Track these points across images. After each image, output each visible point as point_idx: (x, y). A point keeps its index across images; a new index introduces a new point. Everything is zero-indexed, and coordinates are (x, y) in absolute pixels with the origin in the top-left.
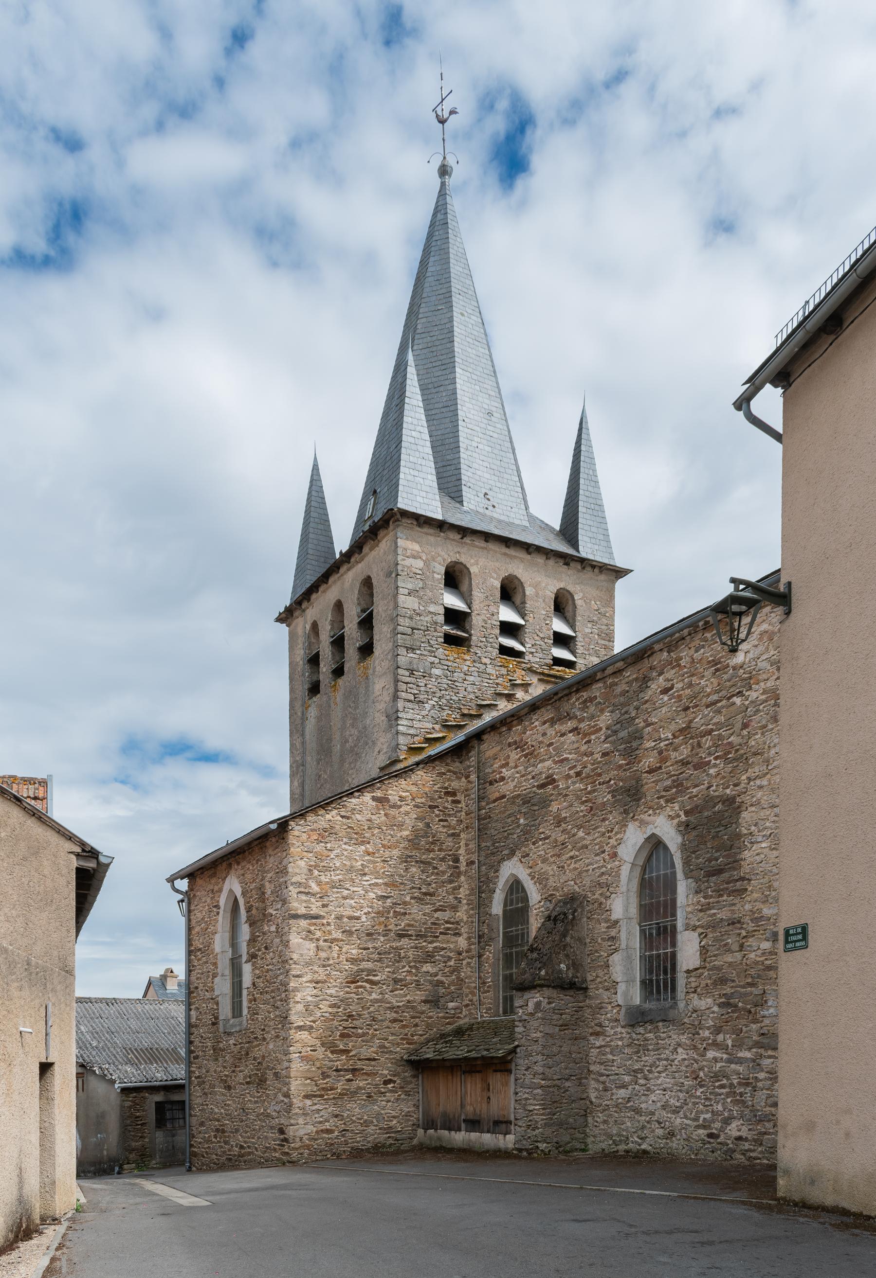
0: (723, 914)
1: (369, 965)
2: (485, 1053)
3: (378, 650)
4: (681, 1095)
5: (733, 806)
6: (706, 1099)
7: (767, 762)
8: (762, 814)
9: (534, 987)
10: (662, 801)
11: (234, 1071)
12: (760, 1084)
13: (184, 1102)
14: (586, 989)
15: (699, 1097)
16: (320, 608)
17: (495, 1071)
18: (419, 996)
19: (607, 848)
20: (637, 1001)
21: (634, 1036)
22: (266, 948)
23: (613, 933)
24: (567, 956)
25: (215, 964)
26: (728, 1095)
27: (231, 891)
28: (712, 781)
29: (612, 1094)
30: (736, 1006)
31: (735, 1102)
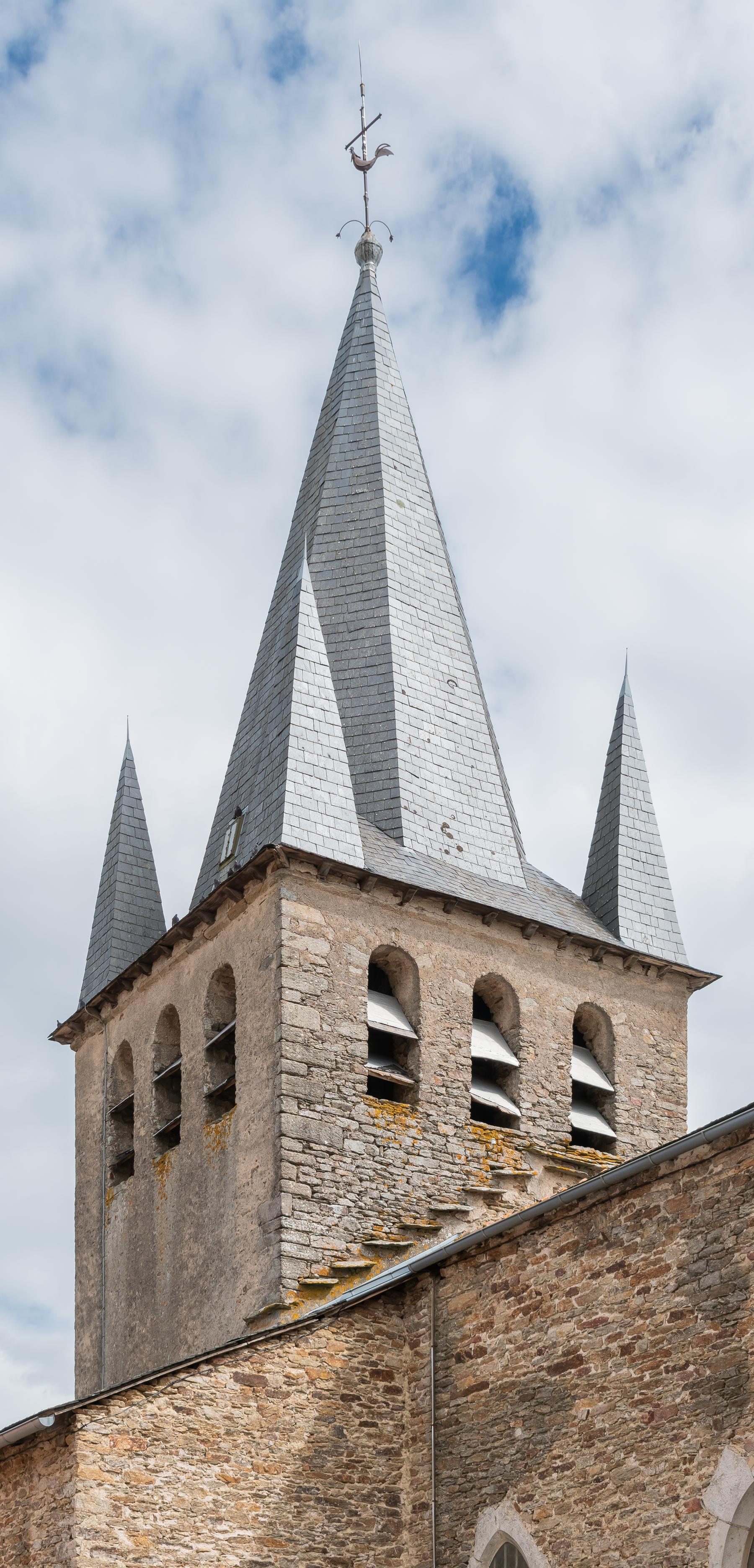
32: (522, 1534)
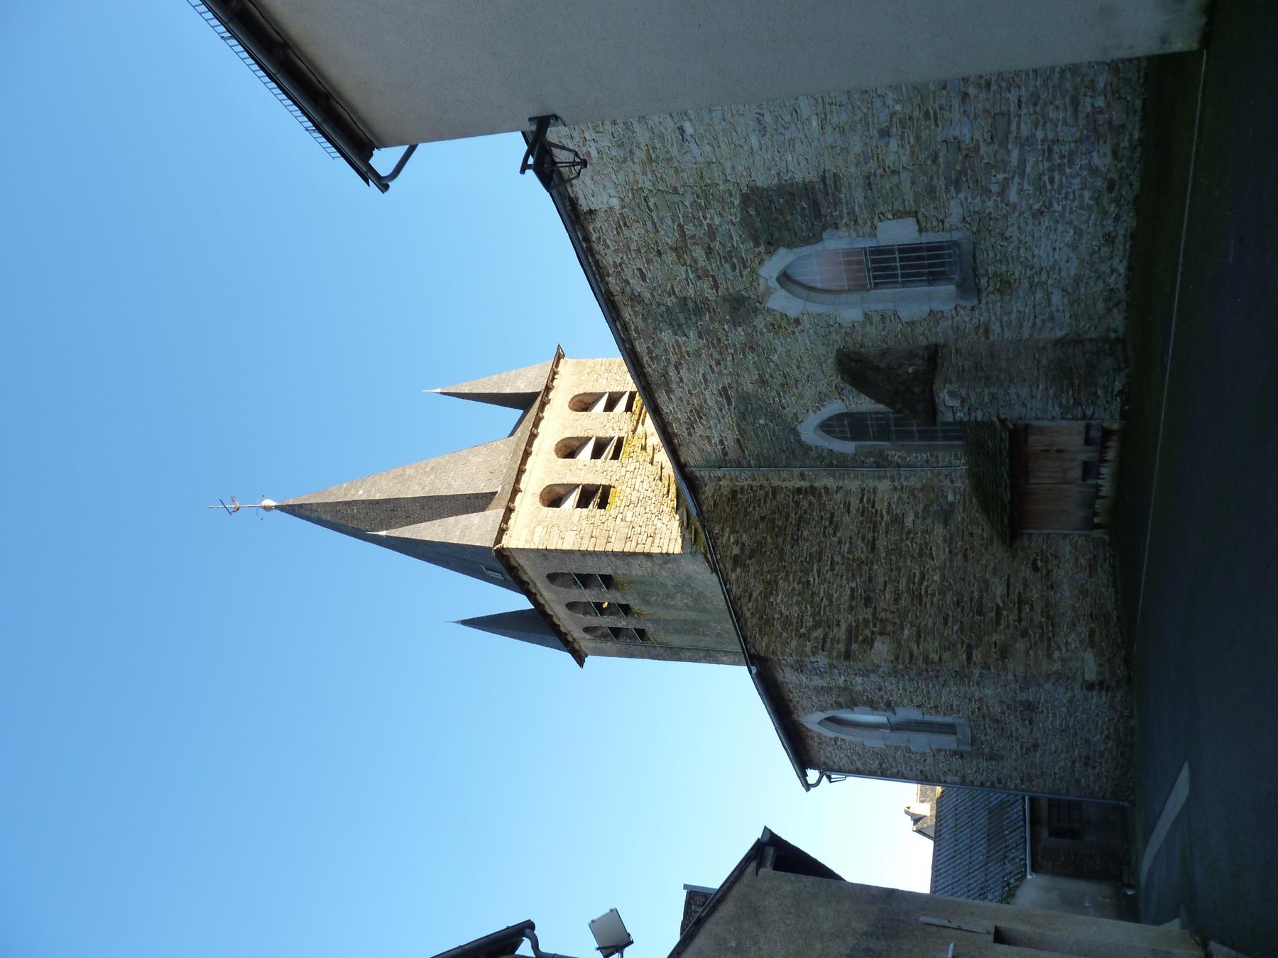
0: (859, 195)
1: (903, 581)
2: (1005, 455)
3: (608, 571)
4: (1061, 228)
5: (752, 197)
6: (1066, 198)
7: (709, 163)
8: (759, 164)
9: (932, 399)
10: (745, 272)
11: (1017, 739)
12: (1050, 136)
13: (1050, 800)
14: (936, 345)
15: (1064, 207)
16: (576, 633)
17: (1026, 442)
18: (939, 530)
19: (790, 330)
20: (951, 288)
21: (991, 289)
22: (880, 689)
23: (876, 318)
24: (900, 365)
25: (897, 749)
26: (1062, 173)
27: (820, 723)
28: (726, 221)
29: (1058, 311)
30: (960, 173)
31: (1071, 163)
32: (814, 419)
